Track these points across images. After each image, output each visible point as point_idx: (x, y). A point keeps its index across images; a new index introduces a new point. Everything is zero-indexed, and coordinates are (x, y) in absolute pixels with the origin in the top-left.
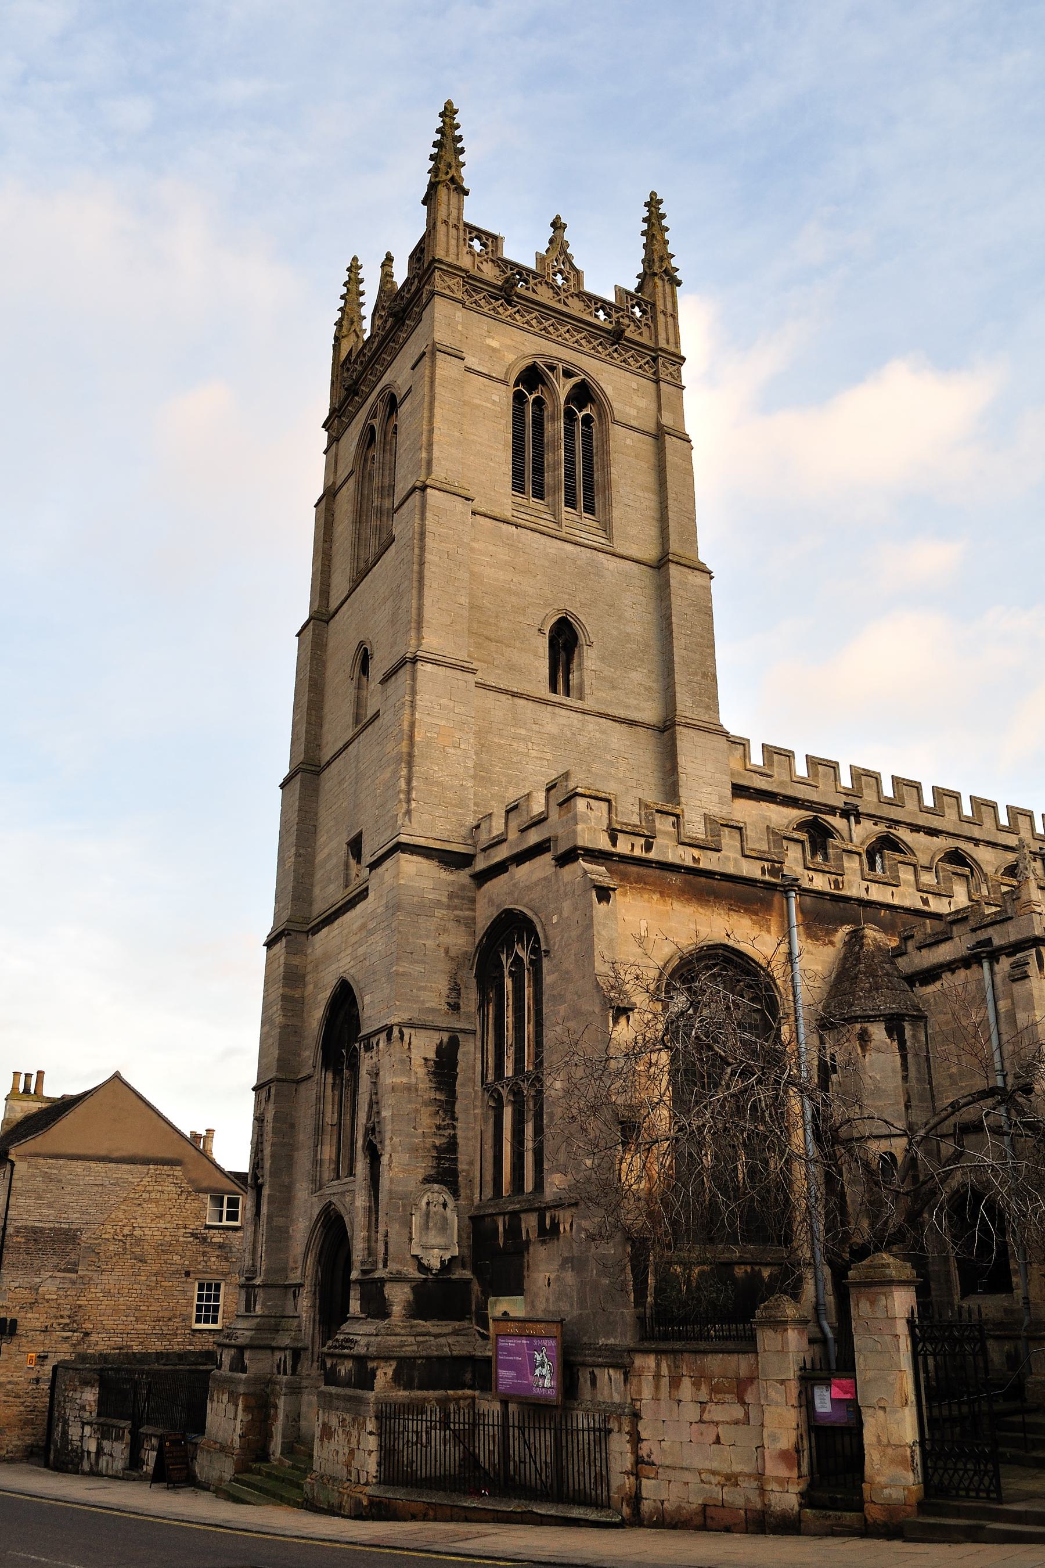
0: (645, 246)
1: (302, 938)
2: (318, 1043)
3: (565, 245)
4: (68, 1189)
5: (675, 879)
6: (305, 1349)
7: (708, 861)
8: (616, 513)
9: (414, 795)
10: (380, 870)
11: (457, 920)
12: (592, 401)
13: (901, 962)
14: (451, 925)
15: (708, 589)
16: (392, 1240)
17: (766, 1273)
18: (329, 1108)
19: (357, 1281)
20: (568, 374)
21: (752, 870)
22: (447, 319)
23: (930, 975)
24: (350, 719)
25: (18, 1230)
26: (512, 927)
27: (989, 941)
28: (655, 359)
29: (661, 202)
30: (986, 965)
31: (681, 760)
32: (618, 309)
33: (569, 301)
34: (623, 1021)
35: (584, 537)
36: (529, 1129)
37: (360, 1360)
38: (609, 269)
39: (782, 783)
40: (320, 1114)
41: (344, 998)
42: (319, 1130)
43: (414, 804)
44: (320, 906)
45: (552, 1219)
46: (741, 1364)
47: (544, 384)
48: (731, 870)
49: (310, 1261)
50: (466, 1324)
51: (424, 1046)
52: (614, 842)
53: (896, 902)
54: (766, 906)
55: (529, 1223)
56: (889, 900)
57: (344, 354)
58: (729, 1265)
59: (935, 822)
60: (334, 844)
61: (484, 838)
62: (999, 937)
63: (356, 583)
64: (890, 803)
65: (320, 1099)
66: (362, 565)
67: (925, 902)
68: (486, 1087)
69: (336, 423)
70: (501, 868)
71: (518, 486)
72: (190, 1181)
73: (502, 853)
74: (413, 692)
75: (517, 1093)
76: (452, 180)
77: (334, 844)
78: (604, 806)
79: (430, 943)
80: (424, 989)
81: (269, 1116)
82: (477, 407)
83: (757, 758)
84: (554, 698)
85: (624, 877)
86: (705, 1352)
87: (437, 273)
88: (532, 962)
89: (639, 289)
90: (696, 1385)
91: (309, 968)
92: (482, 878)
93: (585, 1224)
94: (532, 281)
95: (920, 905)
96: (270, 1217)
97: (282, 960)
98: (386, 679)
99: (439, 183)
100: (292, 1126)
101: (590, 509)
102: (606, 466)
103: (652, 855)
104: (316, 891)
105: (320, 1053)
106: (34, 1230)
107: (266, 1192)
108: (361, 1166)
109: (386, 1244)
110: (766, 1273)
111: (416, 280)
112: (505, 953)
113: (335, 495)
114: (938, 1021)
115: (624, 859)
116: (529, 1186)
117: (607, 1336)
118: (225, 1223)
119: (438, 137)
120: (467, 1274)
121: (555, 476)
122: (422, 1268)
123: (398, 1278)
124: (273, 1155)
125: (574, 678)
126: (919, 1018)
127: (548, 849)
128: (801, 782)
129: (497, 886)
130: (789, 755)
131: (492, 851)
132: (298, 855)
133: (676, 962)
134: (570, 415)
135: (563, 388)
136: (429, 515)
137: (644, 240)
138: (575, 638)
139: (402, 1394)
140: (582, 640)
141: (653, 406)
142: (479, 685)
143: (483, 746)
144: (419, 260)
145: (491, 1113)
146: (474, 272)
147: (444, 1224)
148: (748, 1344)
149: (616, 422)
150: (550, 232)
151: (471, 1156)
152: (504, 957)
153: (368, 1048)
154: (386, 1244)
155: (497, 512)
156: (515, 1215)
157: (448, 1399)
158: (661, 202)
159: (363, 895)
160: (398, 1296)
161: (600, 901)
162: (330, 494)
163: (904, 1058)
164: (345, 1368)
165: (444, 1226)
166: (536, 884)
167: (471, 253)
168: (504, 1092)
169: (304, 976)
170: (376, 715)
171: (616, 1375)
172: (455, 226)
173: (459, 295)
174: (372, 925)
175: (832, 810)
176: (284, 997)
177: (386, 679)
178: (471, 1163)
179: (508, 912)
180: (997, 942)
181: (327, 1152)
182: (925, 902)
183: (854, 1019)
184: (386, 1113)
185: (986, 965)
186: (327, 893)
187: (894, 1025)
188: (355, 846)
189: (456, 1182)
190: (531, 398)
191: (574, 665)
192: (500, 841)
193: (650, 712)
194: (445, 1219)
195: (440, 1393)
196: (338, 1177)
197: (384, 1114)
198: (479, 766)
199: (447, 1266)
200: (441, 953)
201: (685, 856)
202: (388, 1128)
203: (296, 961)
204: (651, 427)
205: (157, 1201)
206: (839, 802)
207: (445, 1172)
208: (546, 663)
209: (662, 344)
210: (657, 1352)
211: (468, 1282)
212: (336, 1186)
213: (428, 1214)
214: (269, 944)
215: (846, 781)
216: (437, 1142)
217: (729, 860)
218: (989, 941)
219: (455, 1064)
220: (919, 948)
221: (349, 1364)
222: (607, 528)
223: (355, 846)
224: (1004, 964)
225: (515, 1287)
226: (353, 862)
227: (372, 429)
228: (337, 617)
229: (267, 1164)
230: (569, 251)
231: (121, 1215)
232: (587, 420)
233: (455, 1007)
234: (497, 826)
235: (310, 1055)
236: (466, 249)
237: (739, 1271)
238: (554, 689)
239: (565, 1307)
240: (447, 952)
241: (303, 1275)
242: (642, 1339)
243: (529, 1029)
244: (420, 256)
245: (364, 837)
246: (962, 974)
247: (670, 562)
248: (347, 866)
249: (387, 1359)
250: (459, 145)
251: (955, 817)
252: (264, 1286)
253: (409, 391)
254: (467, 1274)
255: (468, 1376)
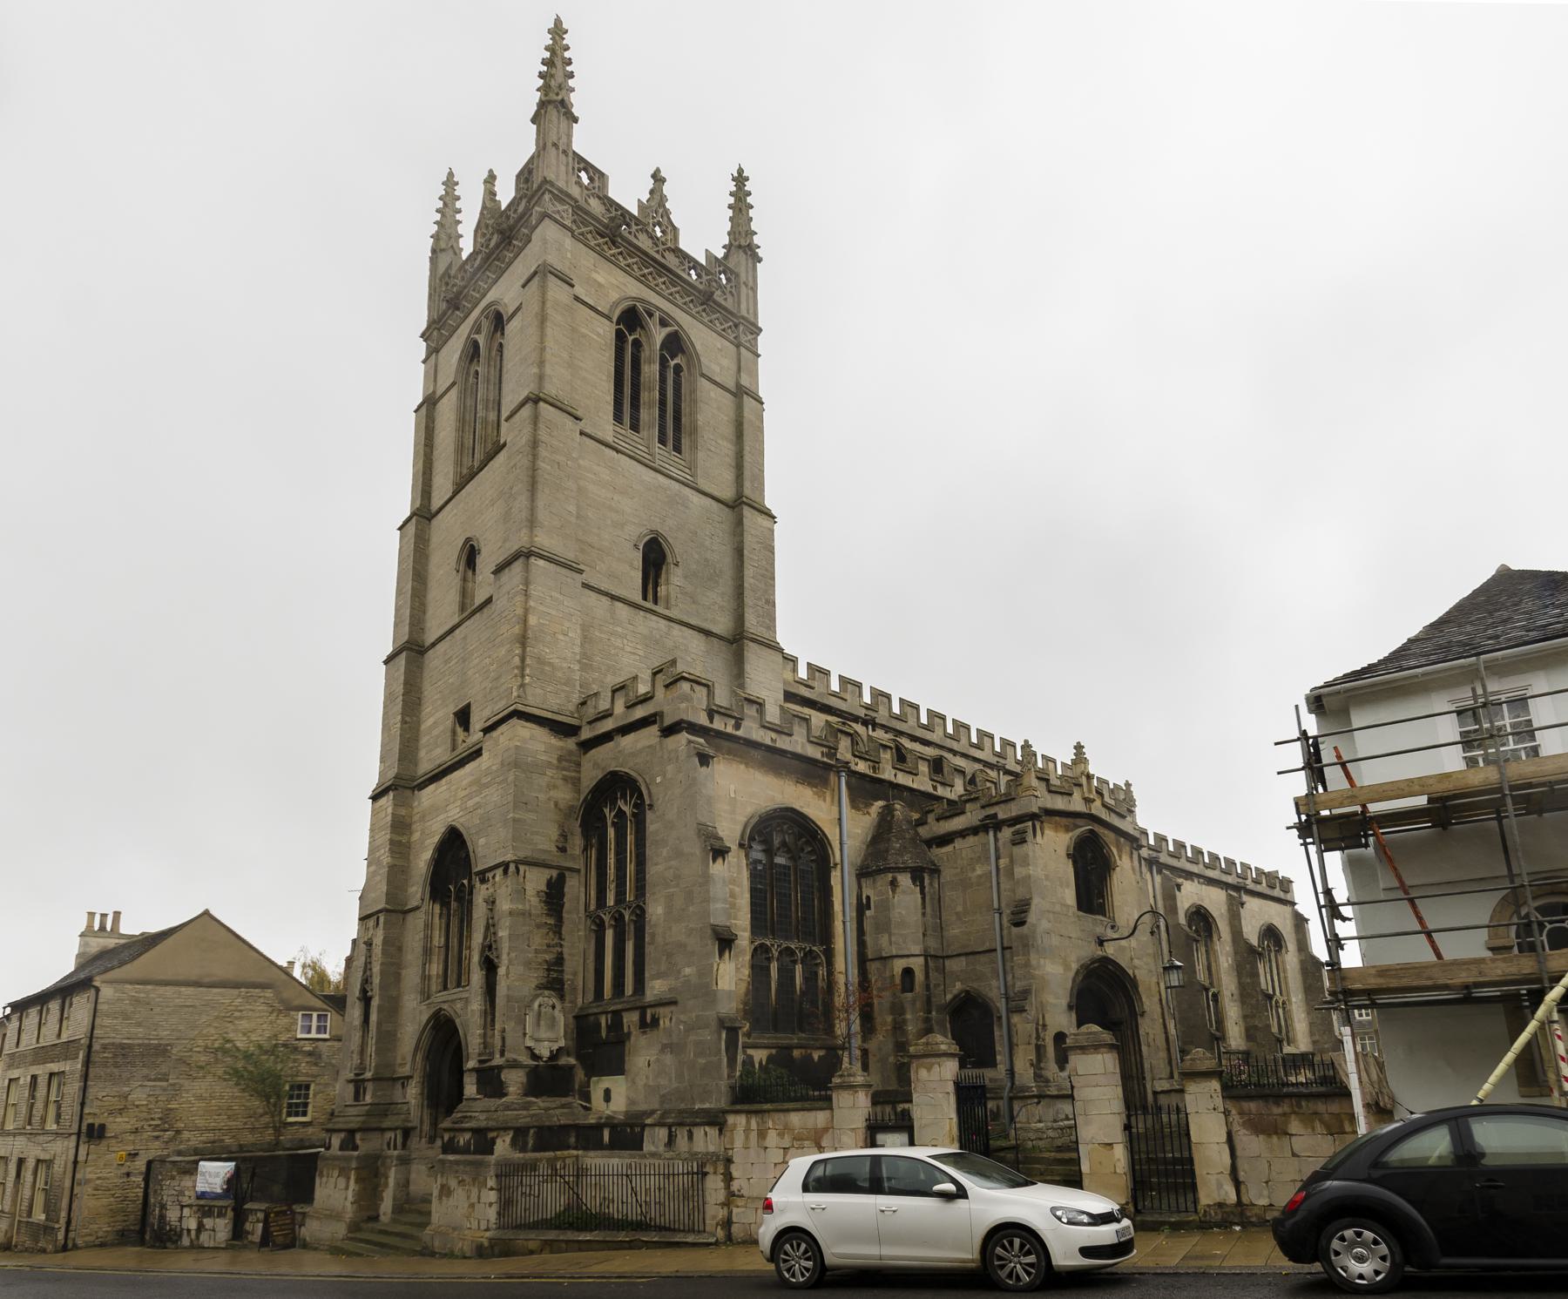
0: (731, 219)
1: (408, 792)
2: (430, 881)
3: (663, 199)
4: (157, 1010)
5: (757, 754)
6: (414, 1128)
7: (783, 743)
8: (701, 455)
9: (528, 671)
10: (495, 734)
11: (565, 779)
12: (683, 352)
13: (921, 830)
14: (560, 782)
15: (772, 531)
16: (508, 1036)
17: (816, 1055)
18: (437, 933)
19: (473, 1070)
20: (663, 323)
21: (815, 753)
22: (551, 242)
23: (945, 840)
24: (456, 607)
25: (105, 1047)
26: (617, 785)
27: (995, 815)
28: (736, 326)
29: (747, 179)
30: (991, 833)
31: (748, 668)
32: (708, 273)
33: (667, 254)
34: (720, 860)
35: (675, 472)
36: (630, 947)
37: (477, 1132)
38: (702, 235)
39: (821, 694)
40: (428, 938)
41: (453, 844)
42: (427, 952)
43: (527, 680)
44: (426, 765)
45: (653, 1016)
46: (820, 1118)
47: (643, 327)
48: (799, 750)
49: (419, 1057)
50: (569, 1099)
51: (536, 881)
52: (711, 720)
53: (915, 786)
54: (824, 782)
55: (630, 1019)
56: (910, 784)
57: (441, 269)
58: (790, 1048)
59: (928, 736)
60: (440, 714)
61: (590, 712)
62: (1002, 813)
63: (459, 488)
64: (897, 718)
65: (428, 926)
66: (465, 471)
67: (935, 788)
68: (588, 915)
69: (436, 334)
70: (607, 737)
71: (618, 417)
72: (282, 1001)
73: (608, 725)
74: (527, 583)
75: (619, 919)
76: (562, 102)
77: (440, 714)
78: (704, 690)
79: (542, 797)
80: (537, 833)
81: (378, 941)
82: (584, 336)
83: (803, 673)
84: (649, 605)
85: (718, 749)
86: (788, 1110)
87: (547, 197)
88: (634, 815)
89: (726, 256)
90: (781, 1135)
91: (416, 818)
92: (587, 746)
93: (682, 1017)
94: (634, 228)
95: (931, 790)
96: (379, 1024)
97: (390, 810)
98: (499, 570)
99: (550, 102)
100: (400, 949)
101: (678, 449)
102: (693, 414)
103: (739, 733)
104: (422, 753)
105: (428, 889)
106: (122, 1046)
107: (375, 1003)
108: (477, 977)
109: (503, 1039)
110: (816, 1055)
111: (524, 202)
112: (610, 810)
113: (435, 404)
114: (947, 874)
115: (720, 734)
116: (629, 989)
117: (702, 1101)
118: (313, 1035)
119: (547, 55)
120: (572, 1061)
121: (649, 415)
122: (535, 1057)
123: (514, 1065)
124: (382, 973)
125: (662, 590)
126: (935, 871)
127: (654, 722)
128: (834, 695)
129: (602, 753)
130: (826, 673)
131: (599, 724)
132: (404, 722)
133: (756, 819)
134: (663, 363)
135: (659, 335)
136: (541, 425)
137: (730, 213)
138: (663, 556)
139: (518, 1155)
140: (669, 559)
141: (734, 368)
142: (586, 586)
143: (586, 639)
144: (527, 181)
145: (593, 935)
146: (582, 203)
147: (553, 1023)
148: (826, 1103)
149: (703, 375)
150: (650, 183)
151: (577, 968)
152: (607, 811)
153: (483, 881)
154: (503, 1039)
155: (599, 435)
156: (617, 1015)
157: (556, 1159)
158: (747, 179)
159: (478, 753)
160: (514, 1081)
161: (702, 764)
162: (429, 405)
163: (923, 899)
164: (462, 1139)
165: (553, 1023)
166: (641, 751)
167: (579, 183)
168: (606, 918)
169: (410, 825)
170: (489, 601)
171: (713, 1132)
172: (564, 152)
173: (568, 223)
174: (484, 781)
175: (856, 719)
176: (392, 842)
177: (499, 570)
178: (575, 974)
179: (614, 774)
180: (1001, 816)
181: (435, 969)
182: (935, 788)
183: (889, 870)
184: (503, 933)
185: (991, 833)
186: (432, 754)
187: (917, 875)
188: (463, 717)
189: (562, 989)
190: (631, 338)
191: (662, 580)
192: (607, 715)
193: (722, 625)
194: (554, 1018)
195: (550, 1154)
196: (445, 988)
197: (500, 934)
198: (584, 655)
199: (554, 1056)
200: (552, 805)
201: (766, 737)
202: (505, 947)
203: (403, 812)
204: (731, 385)
205: (248, 1018)
206: (862, 713)
207: (554, 983)
208: (640, 574)
209: (744, 312)
210: (748, 1112)
211: (571, 1068)
212: (443, 996)
213: (539, 1013)
214: (375, 798)
215: (867, 699)
216: (547, 957)
217: (798, 743)
218: (995, 815)
219: (562, 895)
220: (938, 820)
221: (468, 1136)
222: (692, 467)
223: (463, 717)
224: (1006, 833)
225: (618, 1068)
226: (459, 730)
227: (476, 345)
228: (440, 516)
229: (376, 980)
230: (668, 205)
231: (213, 1031)
232: (678, 369)
233: (563, 850)
234: (604, 704)
235: (416, 891)
236: (575, 179)
237: (796, 1053)
238: (645, 598)
239: (663, 1082)
240: (556, 804)
241: (413, 1069)
242: (734, 1102)
243: (630, 868)
244: (525, 176)
245: (473, 708)
246: (971, 840)
247: (742, 503)
248: (454, 733)
249: (505, 1129)
250: (569, 68)
251: (941, 733)
252: (373, 1079)
253: (518, 309)
254: (572, 1061)
255: (572, 1140)
